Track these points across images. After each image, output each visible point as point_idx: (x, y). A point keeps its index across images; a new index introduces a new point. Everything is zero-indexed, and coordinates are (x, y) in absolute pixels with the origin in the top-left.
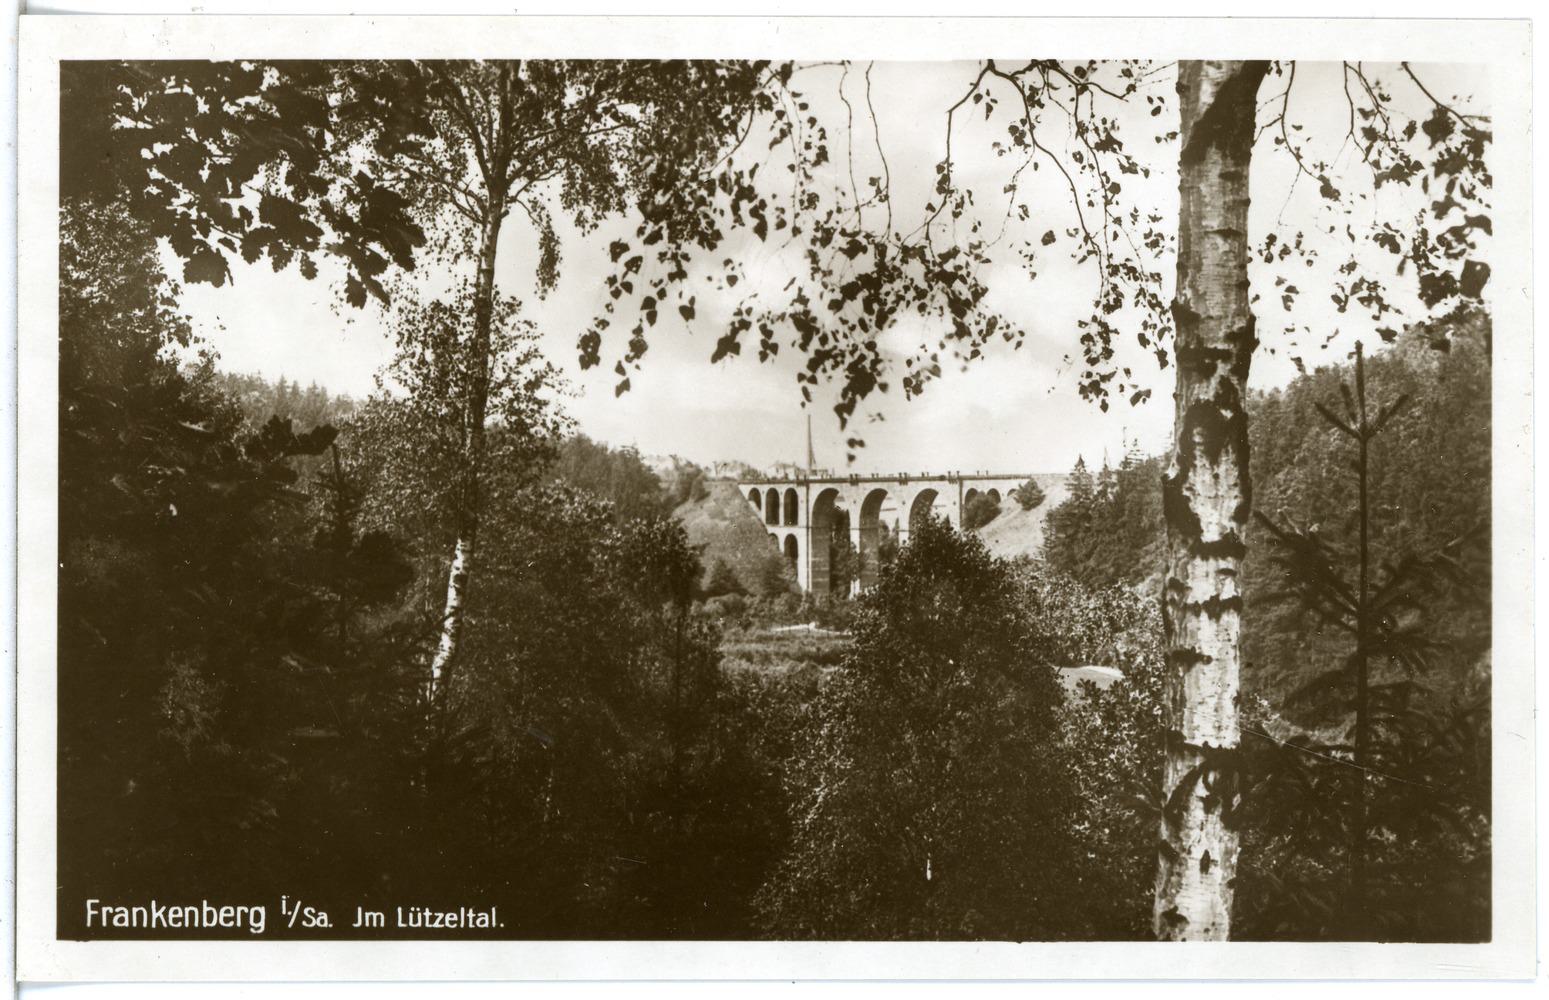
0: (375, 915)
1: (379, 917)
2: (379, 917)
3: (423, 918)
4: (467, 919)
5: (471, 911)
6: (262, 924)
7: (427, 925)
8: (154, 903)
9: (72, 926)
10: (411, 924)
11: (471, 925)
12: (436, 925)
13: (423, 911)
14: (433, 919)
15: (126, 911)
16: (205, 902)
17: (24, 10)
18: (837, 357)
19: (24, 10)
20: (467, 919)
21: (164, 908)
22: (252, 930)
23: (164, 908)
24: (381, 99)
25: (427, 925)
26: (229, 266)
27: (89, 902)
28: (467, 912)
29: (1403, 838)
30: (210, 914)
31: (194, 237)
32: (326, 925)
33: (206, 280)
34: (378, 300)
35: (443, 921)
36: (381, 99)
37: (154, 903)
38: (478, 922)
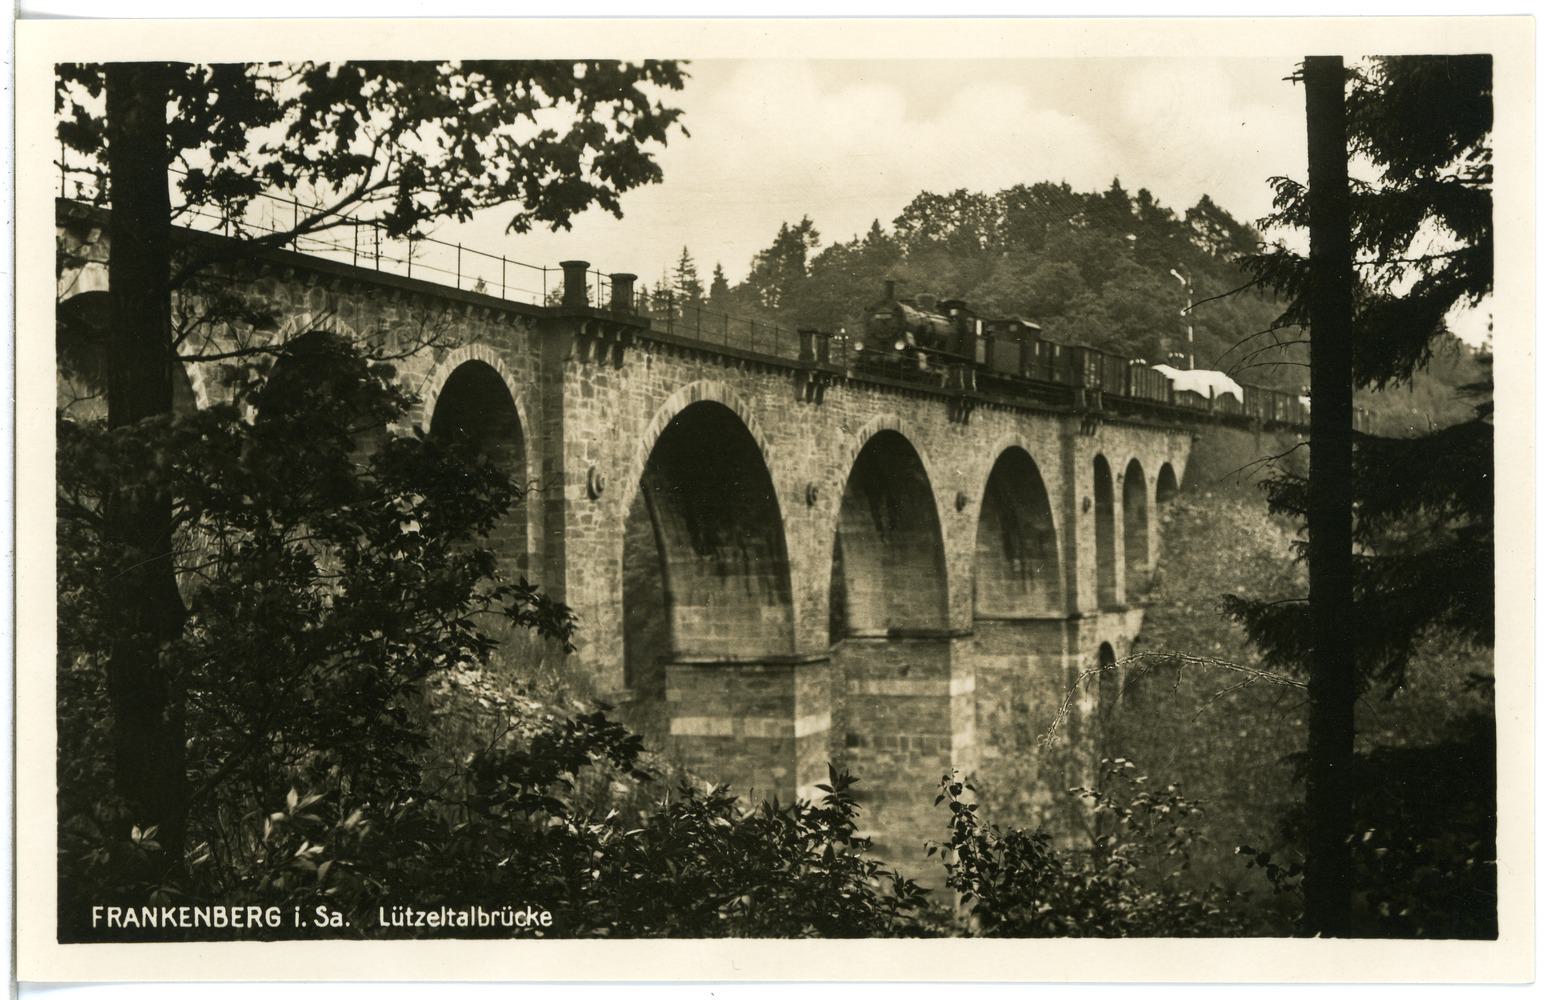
9: (74, 927)
12: (418, 923)
13: (404, 911)
14: (414, 918)
25: (409, 924)
26: (1486, 298)
27: (95, 909)
30: (484, 918)
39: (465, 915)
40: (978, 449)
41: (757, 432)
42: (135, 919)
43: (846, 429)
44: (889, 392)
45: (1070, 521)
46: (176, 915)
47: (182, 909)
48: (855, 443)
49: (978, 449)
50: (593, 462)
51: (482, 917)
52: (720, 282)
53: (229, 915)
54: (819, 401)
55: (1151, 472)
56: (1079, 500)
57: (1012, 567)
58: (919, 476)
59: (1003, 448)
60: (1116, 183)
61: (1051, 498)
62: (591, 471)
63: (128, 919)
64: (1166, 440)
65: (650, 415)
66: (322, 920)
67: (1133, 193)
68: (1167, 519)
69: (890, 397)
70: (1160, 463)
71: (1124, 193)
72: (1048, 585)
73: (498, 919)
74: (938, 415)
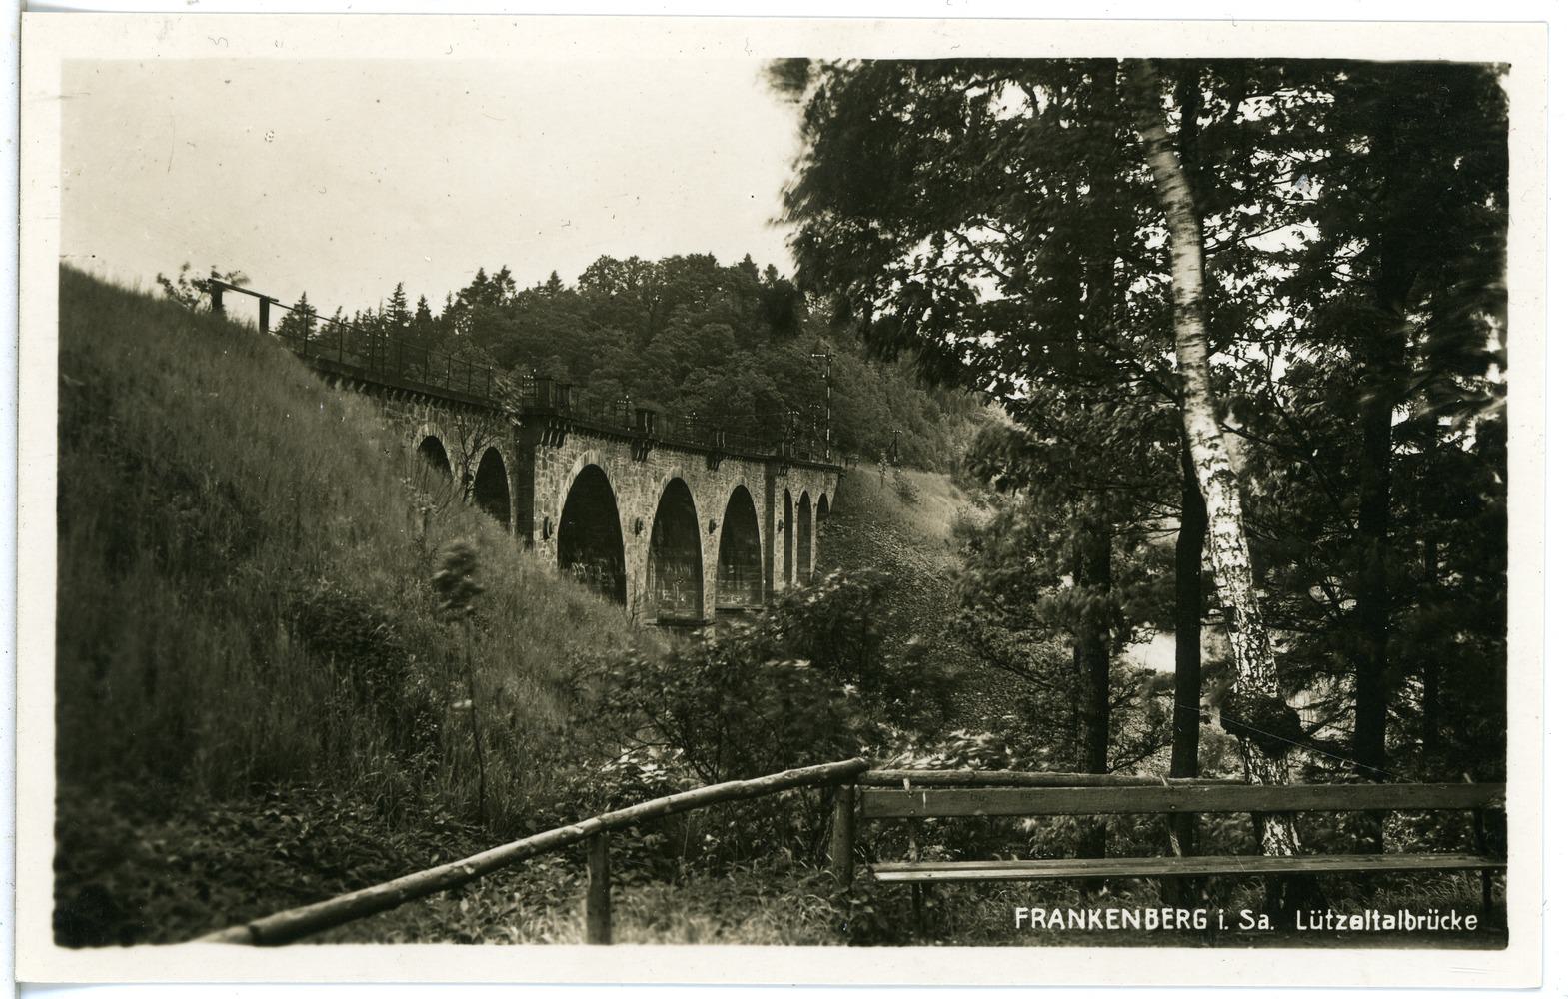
3: (1325, 921)
4: (1372, 921)
5: (1376, 912)
8: (1453, 912)
10: (1313, 927)
11: (1377, 928)
12: (1339, 927)
13: (1325, 914)
17: (25, 8)
18: (393, 388)
19: (25, 8)
20: (1372, 921)
21: (1099, 911)
23: (1099, 911)
29: (1427, 298)
30: (1411, 921)
31: (1244, 230)
32: (1267, 927)
33: (725, 269)
35: (1347, 923)
37: (1453, 912)
38: (1385, 923)
39: (1392, 919)
40: (721, 488)
41: (613, 485)
42: (1060, 920)
43: (655, 479)
45: (769, 538)
46: (1103, 917)
47: (1109, 912)
48: (659, 489)
49: (721, 488)
50: (546, 514)
51: (1410, 921)
52: (423, 311)
53: (1160, 915)
54: (644, 460)
55: (815, 500)
56: (776, 523)
57: (727, 570)
58: (688, 509)
61: (758, 521)
62: (546, 519)
63: (1053, 920)
65: (565, 477)
66: (1247, 923)
68: (822, 534)
69: (678, 453)
72: (753, 585)
73: (1424, 923)
74: (700, 463)
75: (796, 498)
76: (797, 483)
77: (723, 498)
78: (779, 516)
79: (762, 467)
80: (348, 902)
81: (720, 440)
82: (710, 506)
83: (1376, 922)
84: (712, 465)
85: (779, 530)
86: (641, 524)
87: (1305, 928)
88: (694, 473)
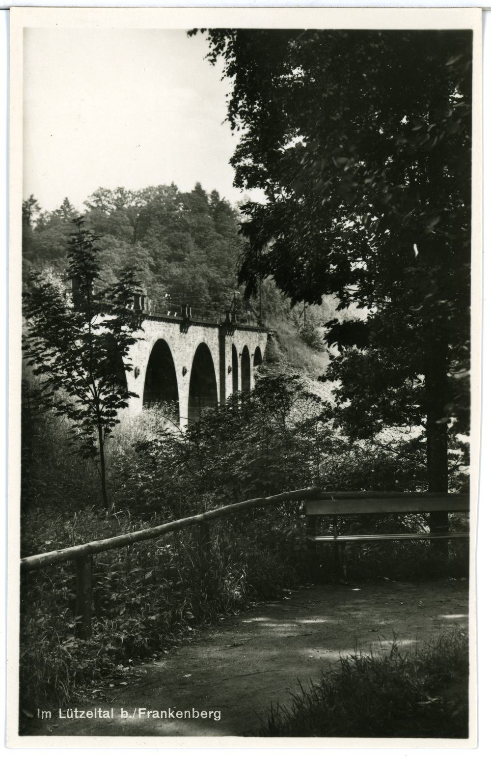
0: (47, 713)
1: (48, 714)
2: (48, 714)
3: (74, 713)
6: (219, 717)
7: (100, 717)
8: (169, 709)
15: (158, 712)
16: (193, 709)
22: (215, 719)
24: (335, 115)
28: (98, 710)
34: (116, 283)
35: (85, 715)
36: (335, 115)
37: (169, 709)
44: (161, 321)
51: (140, 715)
55: (252, 351)
56: (227, 368)
59: (199, 344)
60: (66, 202)
64: (258, 335)
67: (208, 191)
70: (256, 347)
71: (204, 192)
75: (239, 350)
76: (240, 340)
77: (191, 352)
78: (229, 363)
79: (217, 330)
80: (264, 617)
81: (189, 313)
82: (183, 358)
83: (100, 714)
84: (184, 328)
85: (229, 372)
86: (139, 370)
87: (65, 717)
88: (172, 335)
